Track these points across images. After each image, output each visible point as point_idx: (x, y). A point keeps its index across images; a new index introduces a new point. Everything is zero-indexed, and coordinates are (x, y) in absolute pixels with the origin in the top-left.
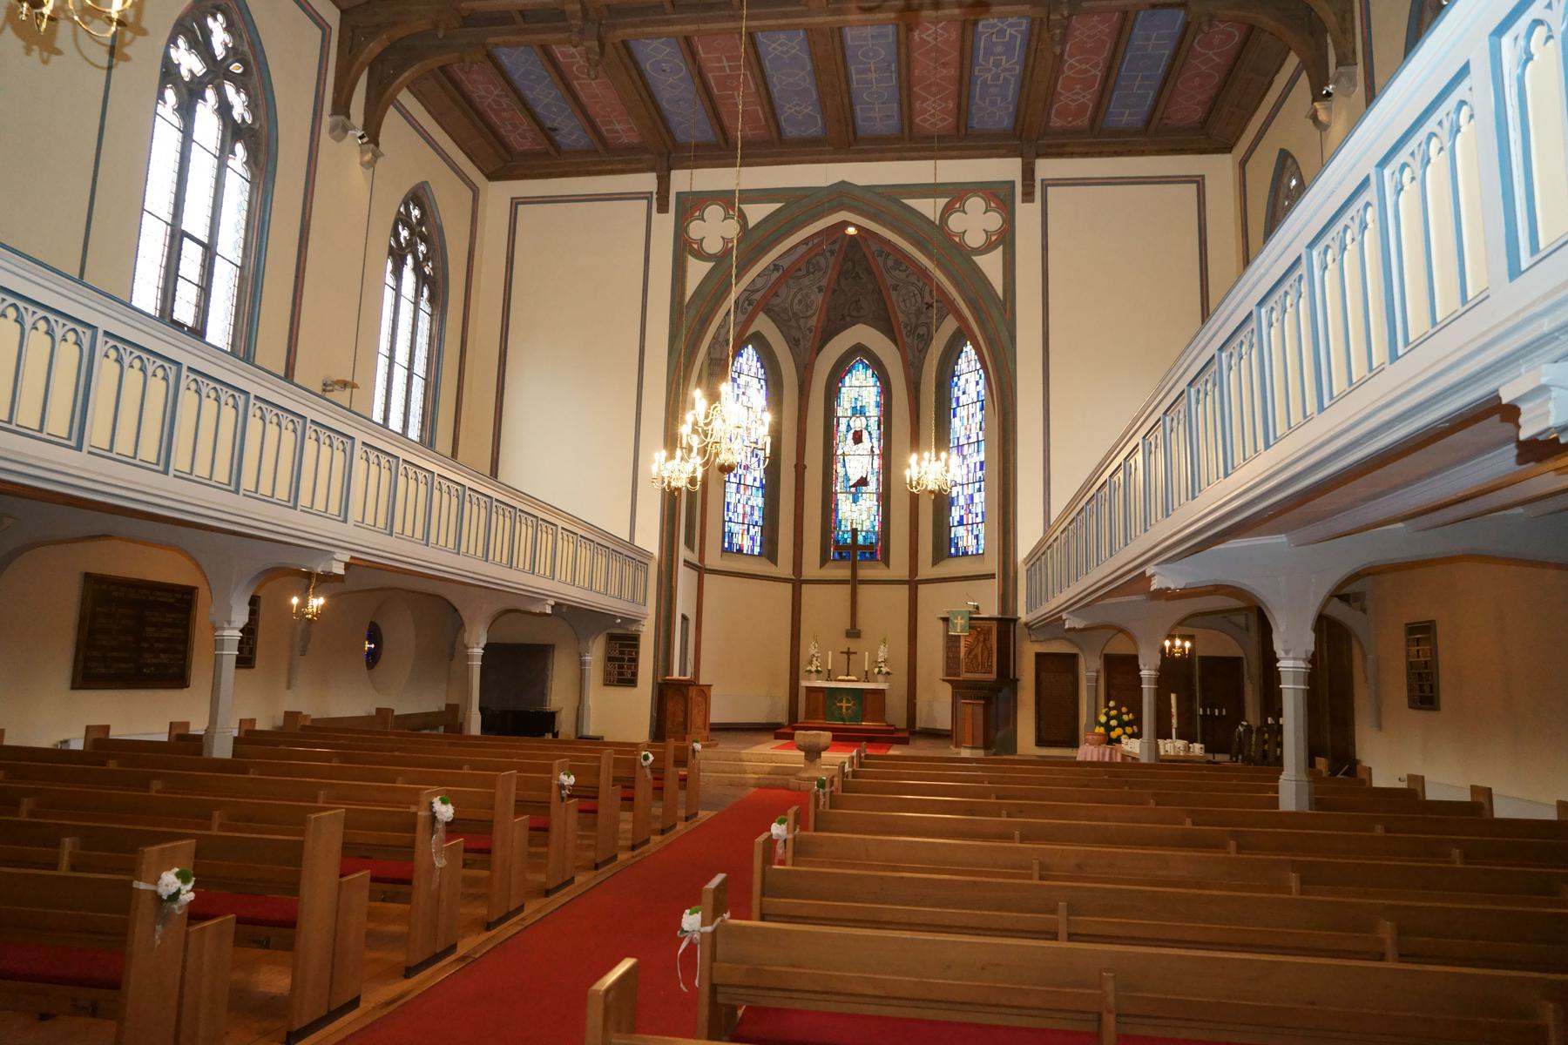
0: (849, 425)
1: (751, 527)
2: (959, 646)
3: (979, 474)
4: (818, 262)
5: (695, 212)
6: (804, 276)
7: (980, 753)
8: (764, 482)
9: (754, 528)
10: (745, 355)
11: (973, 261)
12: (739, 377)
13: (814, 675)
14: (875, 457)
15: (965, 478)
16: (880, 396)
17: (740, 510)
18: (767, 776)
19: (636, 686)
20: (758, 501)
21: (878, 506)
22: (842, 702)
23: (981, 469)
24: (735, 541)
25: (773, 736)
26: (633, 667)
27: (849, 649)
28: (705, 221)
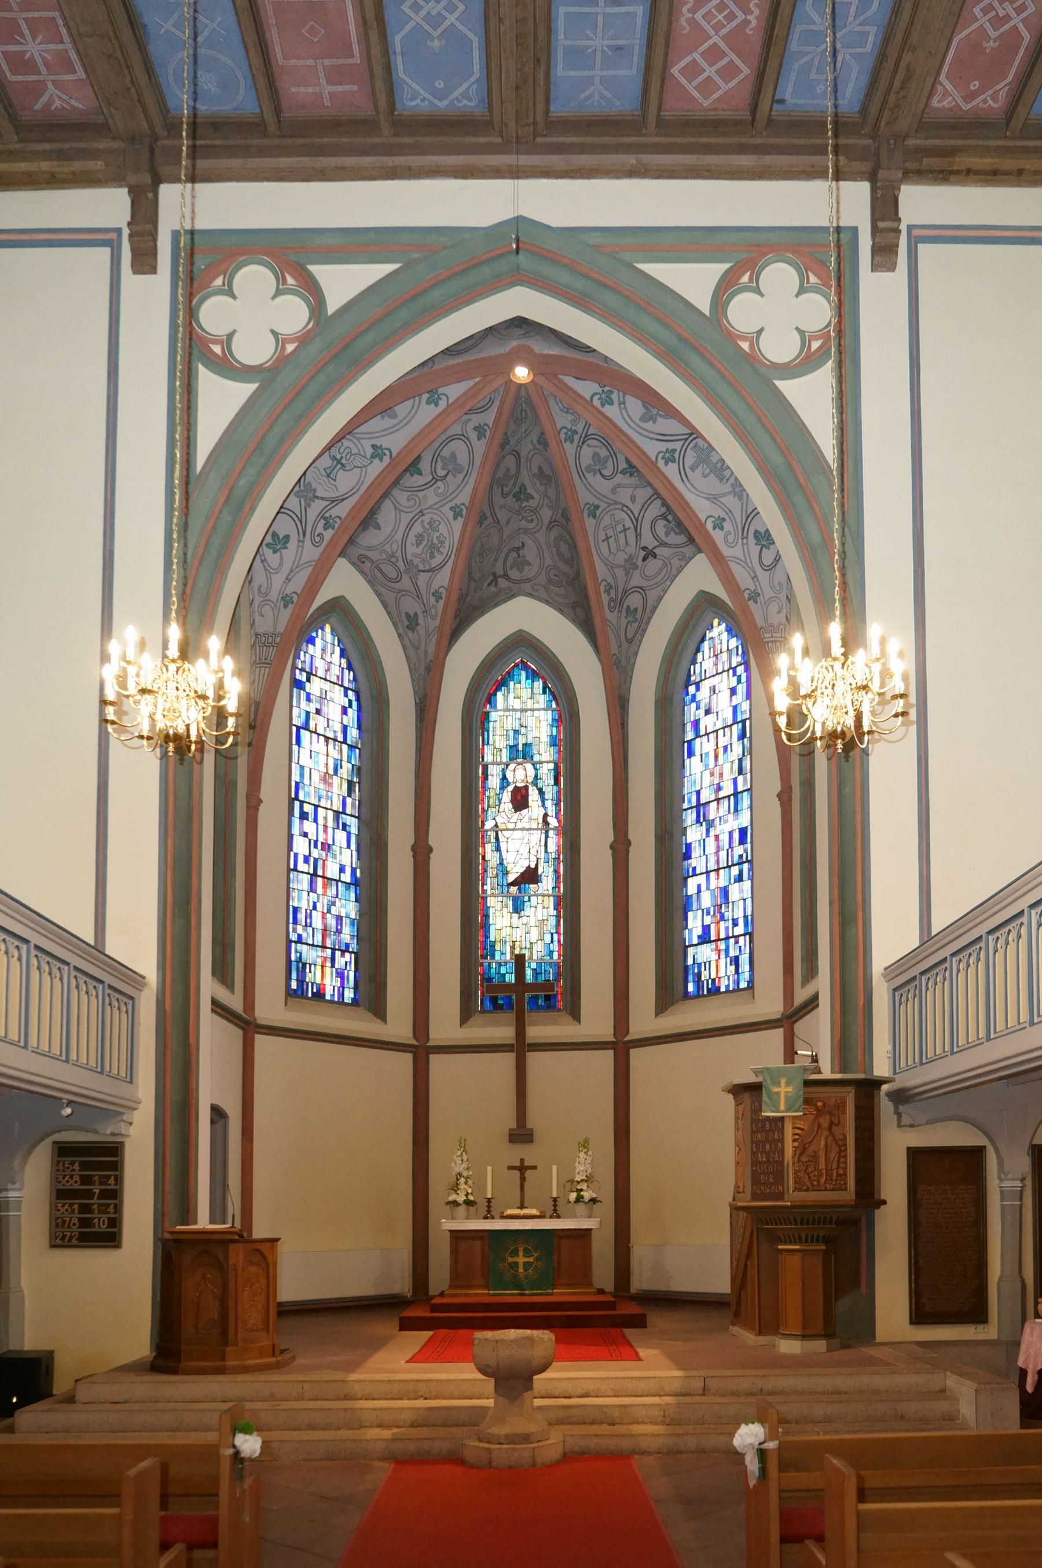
0: (504, 778)
1: (338, 953)
2: (782, 1140)
3: (739, 850)
4: (453, 455)
5: (215, 278)
6: (427, 486)
7: (820, 1346)
8: (358, 875)
9: (343, 955)
10: (318, 641)
11: (774, 384)
12: (308, 680)
13: (462, 1210)
14: (551, 833)
15: (712, 860)
16: (558, 727)
17: (317, 922)
18: (415, 1432)
19: (118, 1246)
20: (348, 907)
21: (558, 917)
22: (517, 1255)
23: (742, 841)
24: (309, 977)
25: (396, 1323)
26: (111, 1209)
27: (522, 1160)
28: (234, 297)
